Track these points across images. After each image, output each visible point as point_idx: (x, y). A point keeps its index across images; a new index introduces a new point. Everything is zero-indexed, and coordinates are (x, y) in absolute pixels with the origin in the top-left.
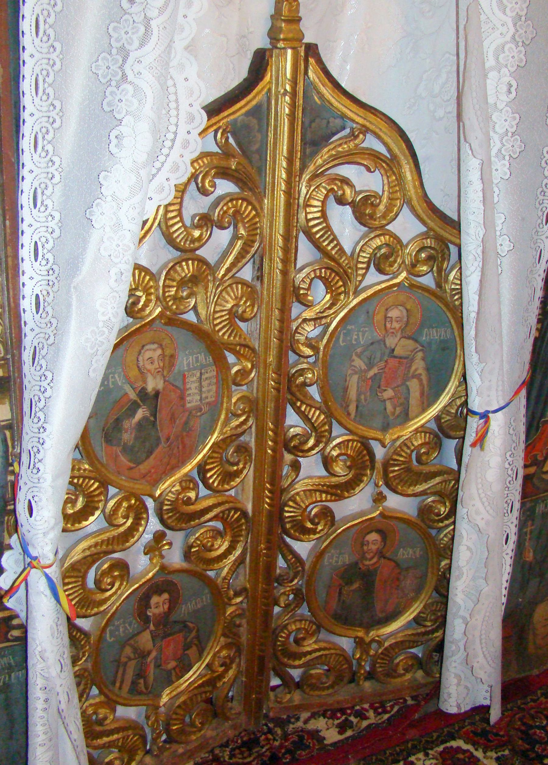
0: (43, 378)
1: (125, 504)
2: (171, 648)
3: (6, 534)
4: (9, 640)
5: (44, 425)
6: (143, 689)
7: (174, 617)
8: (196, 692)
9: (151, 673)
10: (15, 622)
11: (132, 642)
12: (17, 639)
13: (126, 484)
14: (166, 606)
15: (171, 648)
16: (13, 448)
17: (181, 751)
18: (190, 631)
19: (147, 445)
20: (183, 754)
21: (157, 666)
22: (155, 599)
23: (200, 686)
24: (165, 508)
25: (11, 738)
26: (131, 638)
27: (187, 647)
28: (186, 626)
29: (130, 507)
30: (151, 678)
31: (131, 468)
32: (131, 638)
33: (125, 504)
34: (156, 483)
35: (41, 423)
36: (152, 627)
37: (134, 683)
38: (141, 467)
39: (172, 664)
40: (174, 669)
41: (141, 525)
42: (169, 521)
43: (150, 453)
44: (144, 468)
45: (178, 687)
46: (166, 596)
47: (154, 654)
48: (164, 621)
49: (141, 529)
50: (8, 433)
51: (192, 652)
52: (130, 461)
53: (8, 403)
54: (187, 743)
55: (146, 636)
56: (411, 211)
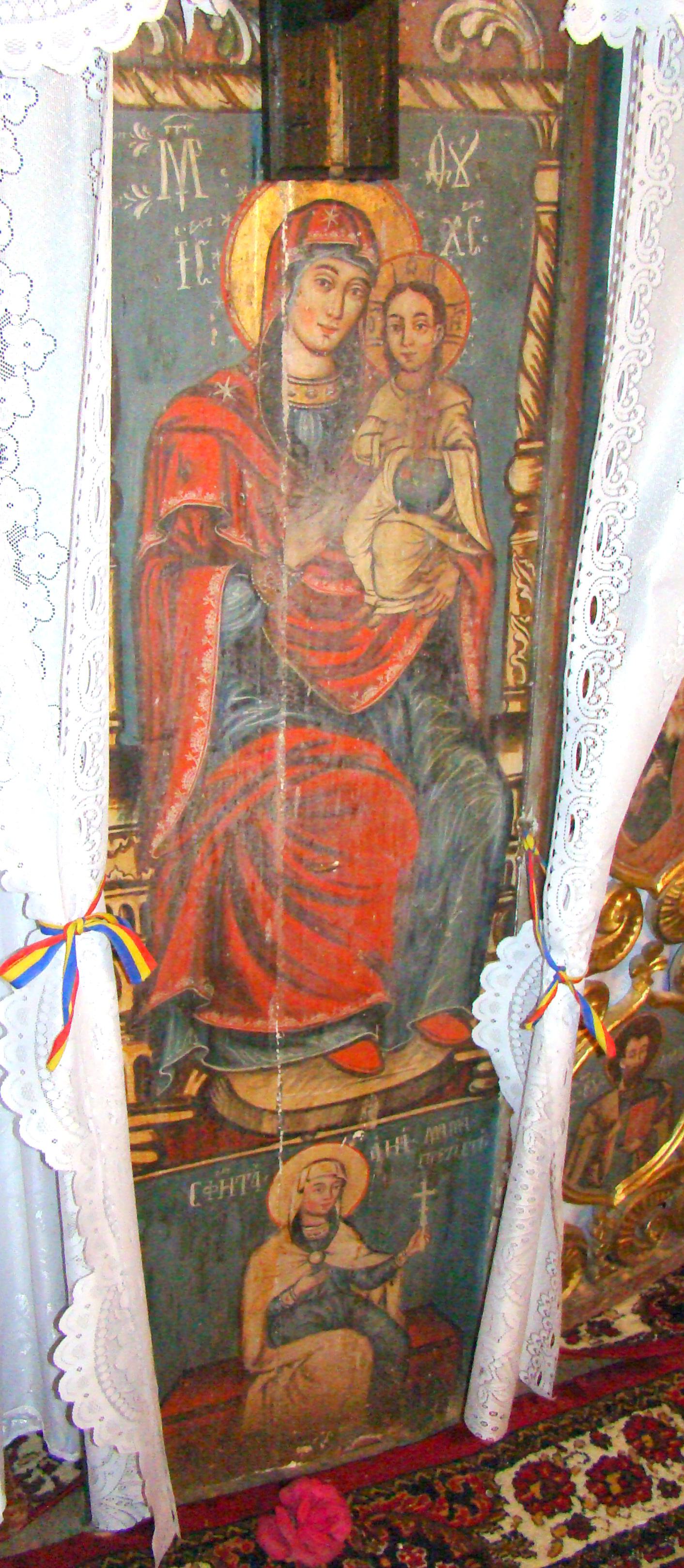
0: (611, 640)
1: (619, 904)
2: (639, 1119)
3: (491, 940)
4: (469, 1094)
5: (606, 707)
6: (596, 1179)
7: (648, 1075)
8: (657, 1187)
9: (611, 1154)
10: (482, 1067)
11: (595, 1107)
12: (480, 1092)
13: (625, 872)
14: (644, 1055)
15: (639, 1119)
16: (519, 814)
17: (626, 1276)
18: (665, 1094)
19: (655, 817)
20: (630, 1281)
21: (619, 1145)
22: (632, 1045)
23: (657, 1182)
24: (664, 909)
25: (446, 1237)
26: (591, 1104)
27: (656, 1120)
28: (661, 1087)
29: (625, 905)
30: (607, 1166)
31: (632, 850)
32: (591, 1104)
33: (619, 904)
34: (656, 871)
35: (601, 703)
36: (622, 1086)
37: (587, 1170)
38: (643, 848)
39: (636, 1143)
40: (637, 1151)
41: (632, 933)
42: (664, 929)
43: (657, 826)
44: (647, 849)
45: (636, 1180)
46: (645, 1040)
47: (617, 1127)
48: (638, 1075)
49: (632, 938)
50: (515, 793)
51: (662, 1125)
52: (633, 840)
53: (521, 750)
54: (634, 1265)
55: (612, 1100)
56: (599, 909)
